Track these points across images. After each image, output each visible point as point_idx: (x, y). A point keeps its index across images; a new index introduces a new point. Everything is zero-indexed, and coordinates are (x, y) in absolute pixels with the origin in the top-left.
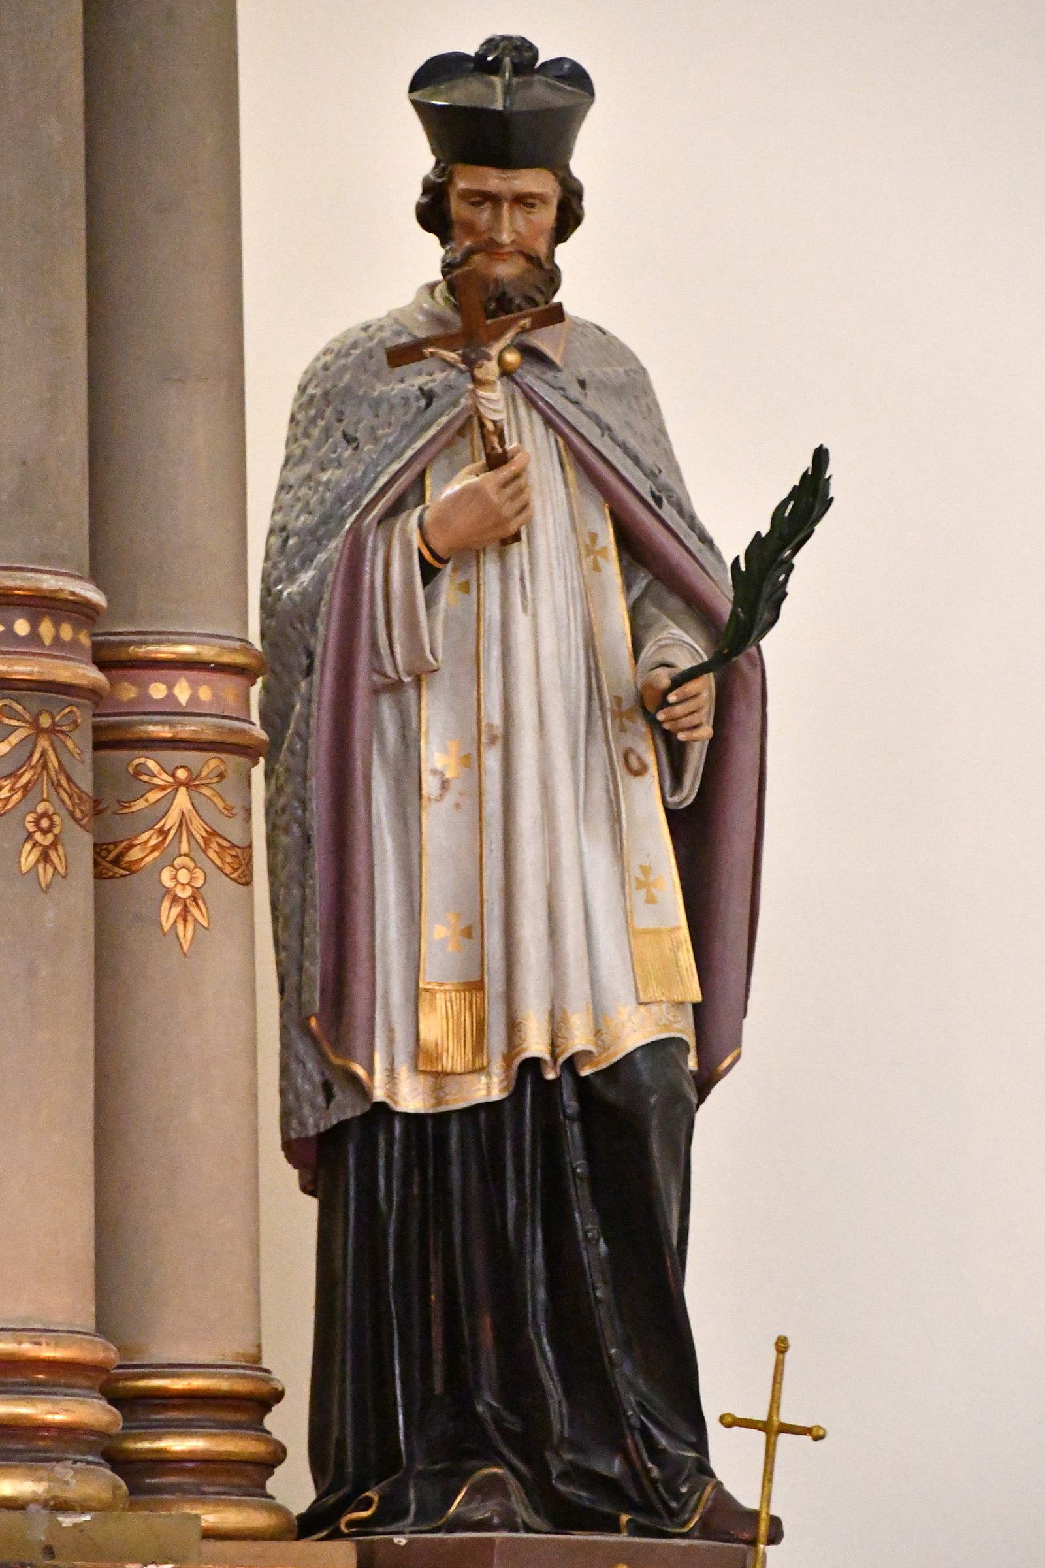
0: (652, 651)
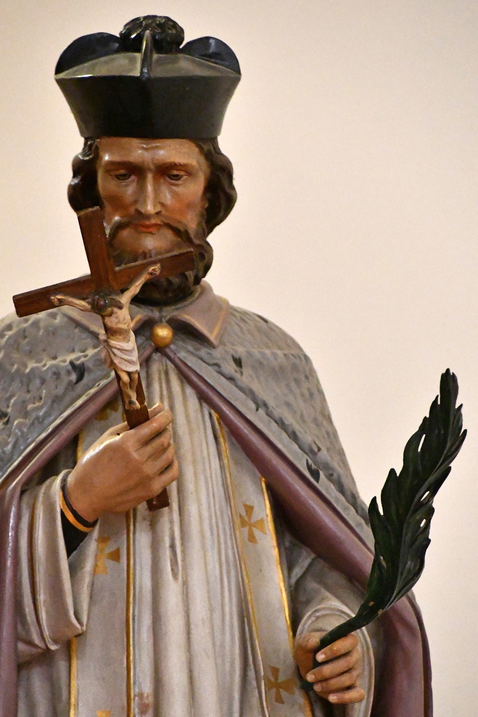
0: (310, 622)
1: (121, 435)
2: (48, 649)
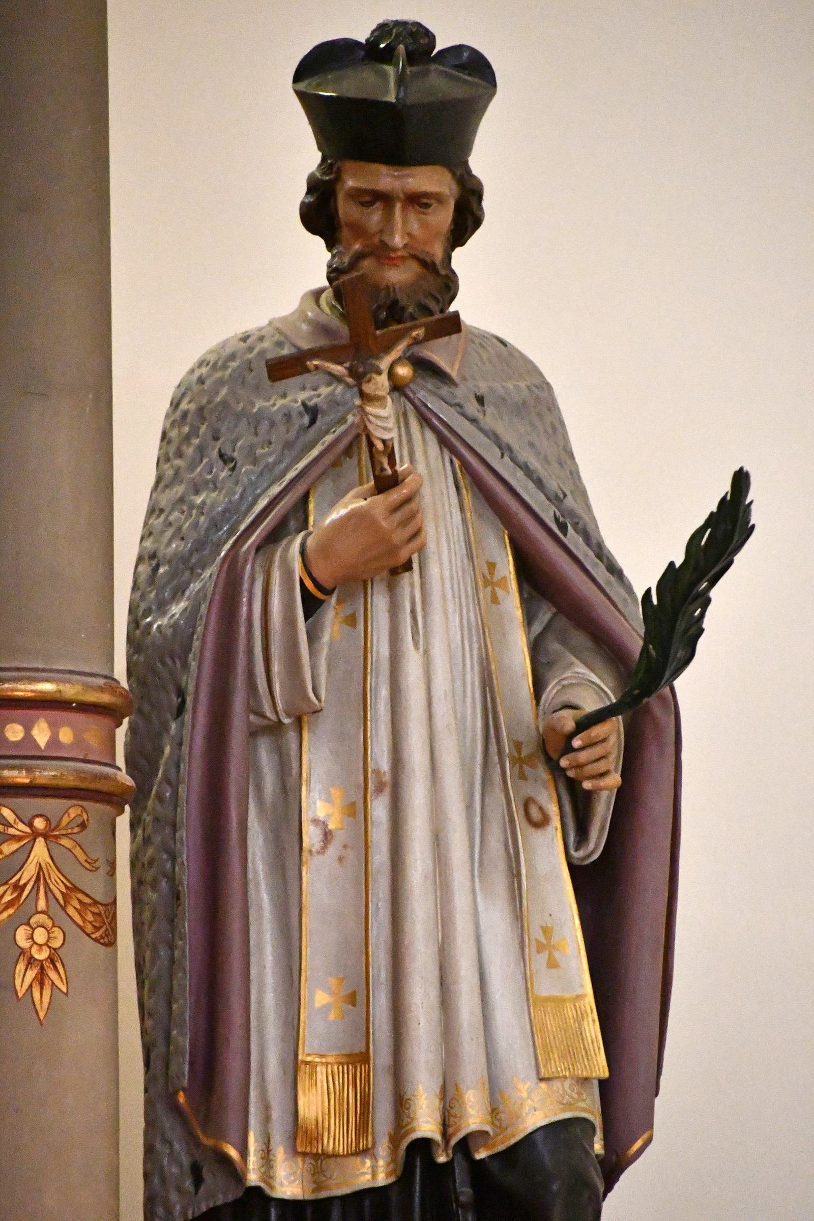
1: (369, 500)
2: (280, 721)
